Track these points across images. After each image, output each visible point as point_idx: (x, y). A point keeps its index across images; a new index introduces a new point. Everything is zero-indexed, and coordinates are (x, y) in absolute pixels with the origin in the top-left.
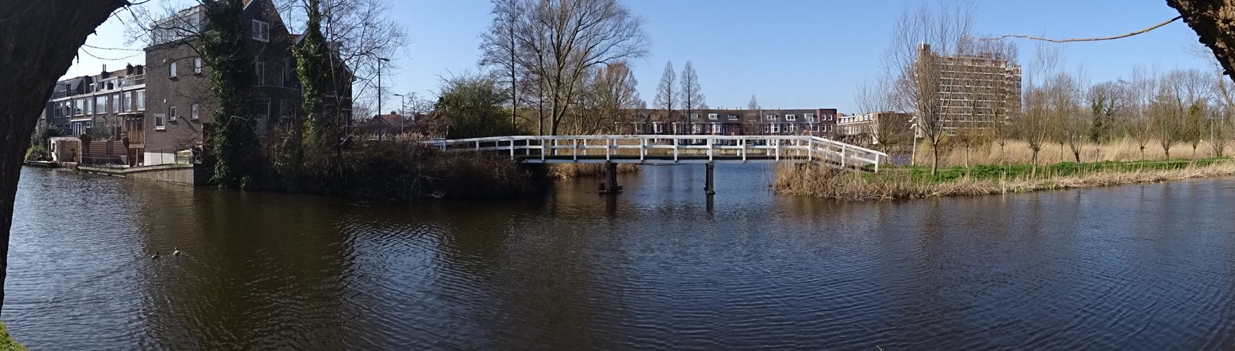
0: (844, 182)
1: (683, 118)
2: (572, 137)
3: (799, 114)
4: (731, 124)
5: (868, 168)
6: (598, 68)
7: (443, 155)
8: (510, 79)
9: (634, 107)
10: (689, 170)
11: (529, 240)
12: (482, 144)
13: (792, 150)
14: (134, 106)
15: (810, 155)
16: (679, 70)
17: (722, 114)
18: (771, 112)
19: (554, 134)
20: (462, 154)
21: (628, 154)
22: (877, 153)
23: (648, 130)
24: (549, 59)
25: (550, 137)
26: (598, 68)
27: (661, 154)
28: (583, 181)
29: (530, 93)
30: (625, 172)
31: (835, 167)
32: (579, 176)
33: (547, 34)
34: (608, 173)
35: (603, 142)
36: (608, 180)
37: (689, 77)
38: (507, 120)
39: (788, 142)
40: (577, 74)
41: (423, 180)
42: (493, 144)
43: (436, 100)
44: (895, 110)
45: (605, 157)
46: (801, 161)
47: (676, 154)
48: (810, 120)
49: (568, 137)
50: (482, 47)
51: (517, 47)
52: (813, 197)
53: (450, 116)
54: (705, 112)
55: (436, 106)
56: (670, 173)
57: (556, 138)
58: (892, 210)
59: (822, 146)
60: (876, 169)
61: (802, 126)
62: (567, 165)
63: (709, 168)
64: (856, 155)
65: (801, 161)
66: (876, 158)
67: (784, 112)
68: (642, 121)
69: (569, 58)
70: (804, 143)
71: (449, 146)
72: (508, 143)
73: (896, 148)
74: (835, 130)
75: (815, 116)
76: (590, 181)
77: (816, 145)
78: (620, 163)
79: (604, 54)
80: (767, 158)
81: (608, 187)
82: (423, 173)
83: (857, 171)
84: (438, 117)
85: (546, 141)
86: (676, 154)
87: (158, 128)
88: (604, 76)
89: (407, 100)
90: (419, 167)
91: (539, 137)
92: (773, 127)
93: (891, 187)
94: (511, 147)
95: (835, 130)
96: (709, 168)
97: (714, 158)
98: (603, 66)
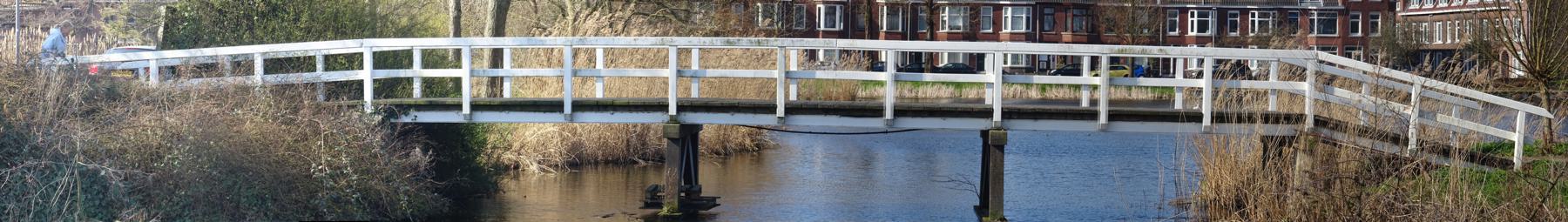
0: (1413, 199)
5: (1490, 155)
10: (925, 152)
12: (273, 65)
13: (1261, 95)
14: (1444, 26)
15: (1309, 111)
19: (457, 33)
20: (210, 95)
22: (1523, 108)
25: (488, 42)
28: (591, 178)
30: (724, 154)
31: (1388, 149)
32: (576, 163)
39: (1241, 69)
41: (91, 179)
42: (307, 63)
46: (1282, 130)
56: (867, 162)
59: (1355, 85)
60: (1517, 157)
62: (537, 130)
63: (992, 147)
64: (1456, 111)
65: (1282, 130)
66: (1518, 125)
70: (1297, 73)
72: (353, 61)
74: (1390, 35)
76: (616, 177)
77: (1331, 80)
78: (710, 124)
80: (1174, 117)
82: (89, 155)
83: (1457, 164)
85: (476, 55)
95: (1390, 35)
96: (992, 147)
97: (1008, 114)
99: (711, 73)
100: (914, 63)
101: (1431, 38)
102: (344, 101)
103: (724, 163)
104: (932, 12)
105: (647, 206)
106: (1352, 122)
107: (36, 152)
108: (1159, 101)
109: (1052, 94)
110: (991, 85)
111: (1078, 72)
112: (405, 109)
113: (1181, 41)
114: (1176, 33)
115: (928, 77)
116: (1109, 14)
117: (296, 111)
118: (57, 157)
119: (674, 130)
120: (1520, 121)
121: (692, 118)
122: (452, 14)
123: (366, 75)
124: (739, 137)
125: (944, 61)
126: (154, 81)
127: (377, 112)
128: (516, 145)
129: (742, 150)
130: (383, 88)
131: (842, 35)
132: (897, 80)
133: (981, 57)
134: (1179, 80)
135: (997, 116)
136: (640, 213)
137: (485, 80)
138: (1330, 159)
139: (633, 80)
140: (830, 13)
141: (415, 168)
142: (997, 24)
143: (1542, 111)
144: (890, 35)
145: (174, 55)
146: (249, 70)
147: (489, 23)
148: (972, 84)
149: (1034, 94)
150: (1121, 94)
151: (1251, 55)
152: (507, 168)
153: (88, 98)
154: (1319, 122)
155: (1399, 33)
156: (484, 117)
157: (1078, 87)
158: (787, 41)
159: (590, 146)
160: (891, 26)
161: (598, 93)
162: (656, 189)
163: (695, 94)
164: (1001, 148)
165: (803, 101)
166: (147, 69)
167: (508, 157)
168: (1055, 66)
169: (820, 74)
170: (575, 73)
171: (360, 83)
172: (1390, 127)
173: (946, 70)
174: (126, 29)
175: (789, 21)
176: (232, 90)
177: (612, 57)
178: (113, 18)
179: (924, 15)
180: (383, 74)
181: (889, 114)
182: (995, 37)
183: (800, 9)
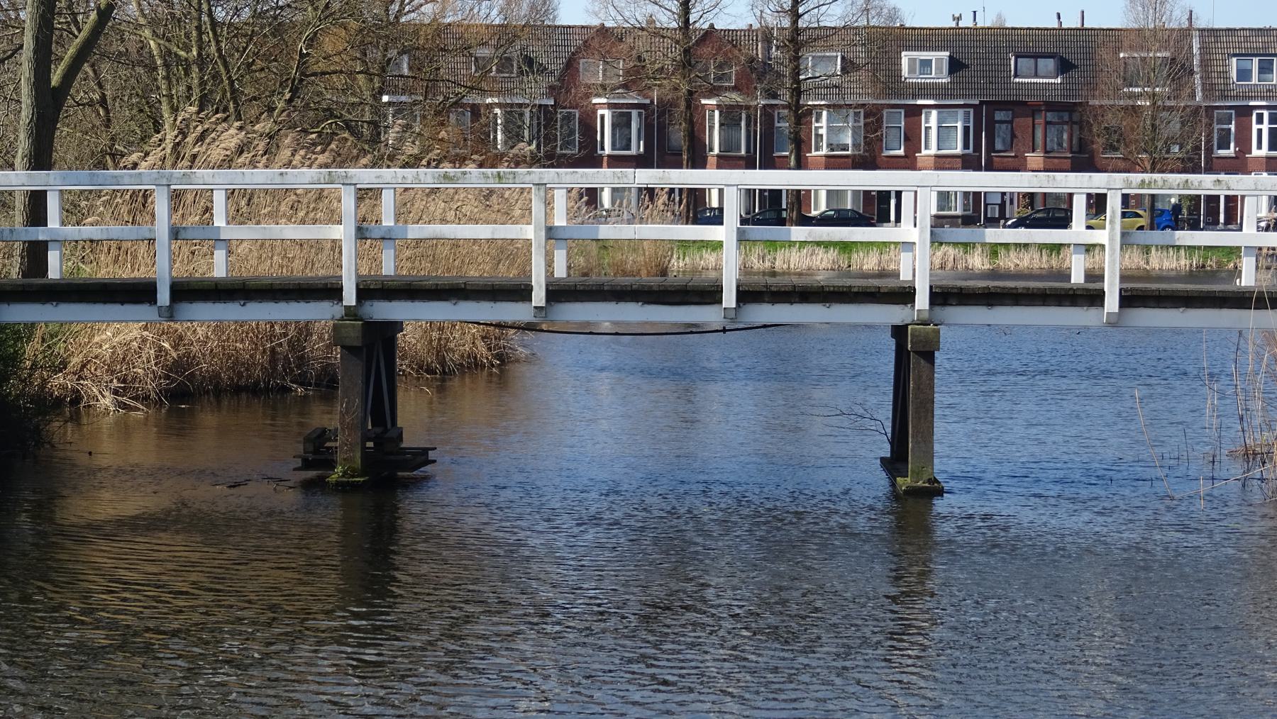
1: (757, 72)
4: (1023, 107)
17: (976, 56)
19: (41, 159)
21: (474, 273)
28: (208, 419)
30: (443, 372)
32: (183, 394)
35: (317, 205)
45: (332, 291)
47: (730, 272)
57: (53, 182)
62: (115, 333)
63: (913, 355)
78: (414, 320)
80: (1241, 300)
81: (347, 460)
87: (1222, 152)
96: (913, 355)
97: (940, 297)
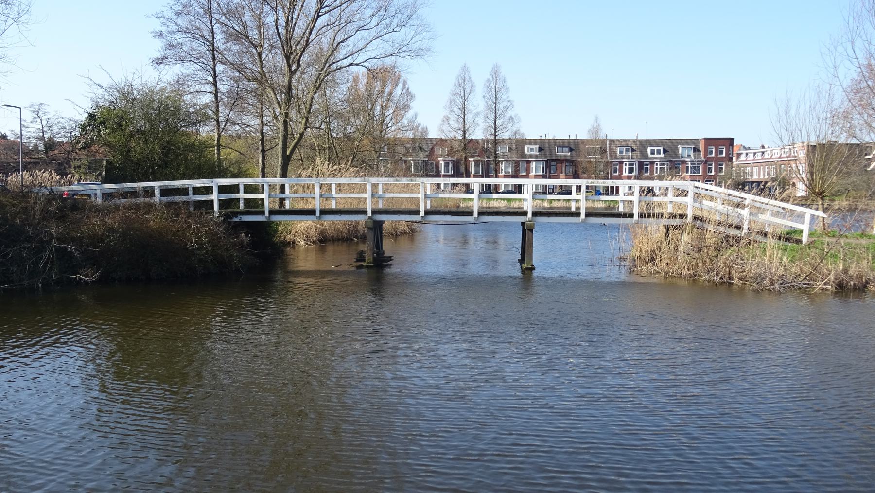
1: (484, 151)
2: (313, 180)
3: (670, 147)
4: (559, 161)
5: (790, 237)
6: (351, 77)
7: (96, 209)
8: (210, 88)
9: (410, 135)
11: (236, 344)
12: (165, 192)
13: (660, 204)
14: (764, 169)
16: (480, 78)
17: (545, 147)
18: (625, 144)
19: (263, 177)
20: (128, 208)
22: (808, 212)
23: (430, 169)
24: (275, 59)
25: (278, 181)
26: (351, 77)
27: (450, 206)
28: (330, 248)
29: (244, 111)
30: (396, 235)
32: (324, 241)
33: (270, 19)
34: (370, 236)
36: (369, 252)
37: (496, 90)
38: (208, 152)
39: (650, 190)
40: (318, 84)
41: (62, 254)
42: (184, 191)
43: (83, 117)
44: (843, 139)
45: (365, 212)
47: (476, 207)
48: (686, 154)
49: (304, 181)
50: (161, 35)
51: (219, 36)
52: (693, 279)
53: (108, 145)
54: (520, 144)
55: (83, 128)
58: (833, 304)
59: (712, 199)
60: (805, 238)
61: (675, 167)
62: (304, 224)
63: (527, 231)
64: (770, 214)
65: (677, 222)
66: (806, 220)
67: (643, 144)
68: (424, 157)
69: (305, 59)
70: (684, 193)
71: (107, 196)
72: (208, 190)
73: (841, 203)
75: (696, 150)
76: (343, 247)
78: (388, 221)
79: (361, 53)
80: (619, 215)
81: (369, 258)
83: (771, 241)
84: (86, 146)
86: (476, 207)
88: (361, 86)
89: (28, 116)
90: (53, 230)
91: (259, 181)
92: (626, 167)
93: (833, 269)
94: (215, 197)
95: (729, 175)
96: (527, 231)
97: (535, 214)
98: (361, 70)
99: (388, 195)
100: (488, 189)
101: (752, 176)
102: (203, 211)
103: (395, 240)
104: (496, 165)
105: (358, 261)
106: (713, 217)
107: (29, 239)
108: (608, 208)
109: (555, 204)
110: (526, 200)
111: (570, 194)
112: (236, 214)
113: (620, 177)
114: (617, 174)
115: (495, 196)
116: (584, 165)
117: (178, 216)
118: (42, 241)
119: (371, 225)
120: (807, 219)
121: (379, 218)
122: (260, 168)
123: (215, 197)
124: (403, 227)
125: (502, 189)
126: (99, 201)
127: (221, 216)
128: (293, 231)
129: (405, 233)
130: (223, 204)
131: (452, 176)
132: (479, 198)
133: (520, 186)
134: (620, 197)
135: (530, 215)
136: (355, 264)
137: (277, 200)
138: (701, 237)
139: (348, 198)
140: (447, 165)
141: (241, 243)
142: (528, 170)
143: (820, 213)
144: (475, 176)
145: (110, 187)
146: (153, 194)
147: (279, 171)
148: (516, 200)
149: (546, 204)
150: (590, 204)
151: (655, 184)
152: (289, 242)
153: (60, 209)
154: (696, 218)
155: (734, 173)
156: (276, 218)
157: (569, 201)
158: (425, 179)
159: (330, 232)
160: (477, 171)
161: (333, 205)
162: (362, 252)
163: (380, 205)
164: (531, 231)
165: (433, 209)
166: (96, 194)
167: (289, 237)
168: (557, 191)
169: (441, 195)
170: (321, 196)
171: (212, 201)
172: (735, 222)
173: (503, 193)
174: (86, 174)
175: (426, 170)
176: (143, 205)
177: (340, 188)
178: (79, 167)
179: (492, 166)
180: (224, 197)
181: (476, 214)
182: (527, 176)
183: (432, 164)
